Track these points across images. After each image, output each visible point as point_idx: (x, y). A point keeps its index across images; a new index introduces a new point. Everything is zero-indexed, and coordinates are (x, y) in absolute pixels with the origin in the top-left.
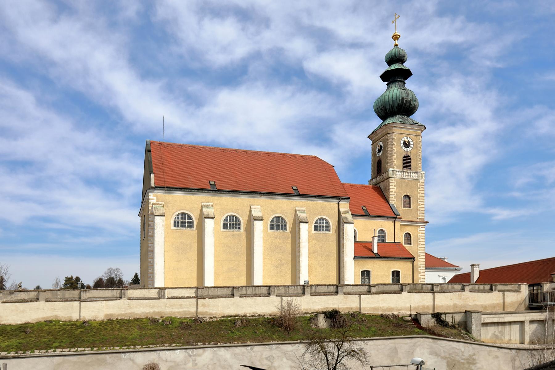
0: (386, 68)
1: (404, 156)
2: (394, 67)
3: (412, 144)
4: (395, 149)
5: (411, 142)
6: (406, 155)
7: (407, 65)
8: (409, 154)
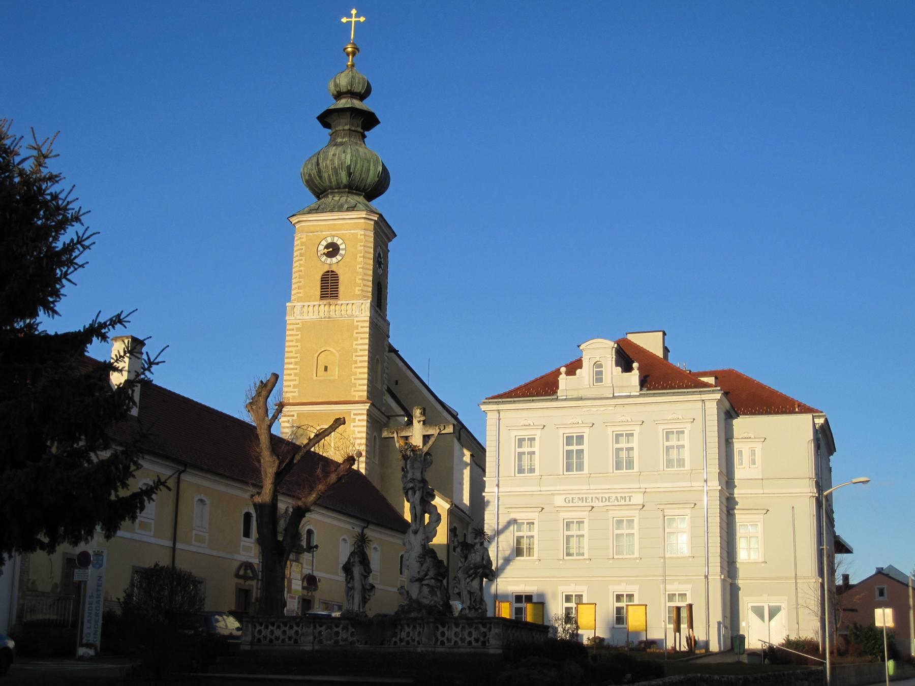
1: (323, 275)
3: (343, 250)
6: (328, 272)
8: (334, 268)
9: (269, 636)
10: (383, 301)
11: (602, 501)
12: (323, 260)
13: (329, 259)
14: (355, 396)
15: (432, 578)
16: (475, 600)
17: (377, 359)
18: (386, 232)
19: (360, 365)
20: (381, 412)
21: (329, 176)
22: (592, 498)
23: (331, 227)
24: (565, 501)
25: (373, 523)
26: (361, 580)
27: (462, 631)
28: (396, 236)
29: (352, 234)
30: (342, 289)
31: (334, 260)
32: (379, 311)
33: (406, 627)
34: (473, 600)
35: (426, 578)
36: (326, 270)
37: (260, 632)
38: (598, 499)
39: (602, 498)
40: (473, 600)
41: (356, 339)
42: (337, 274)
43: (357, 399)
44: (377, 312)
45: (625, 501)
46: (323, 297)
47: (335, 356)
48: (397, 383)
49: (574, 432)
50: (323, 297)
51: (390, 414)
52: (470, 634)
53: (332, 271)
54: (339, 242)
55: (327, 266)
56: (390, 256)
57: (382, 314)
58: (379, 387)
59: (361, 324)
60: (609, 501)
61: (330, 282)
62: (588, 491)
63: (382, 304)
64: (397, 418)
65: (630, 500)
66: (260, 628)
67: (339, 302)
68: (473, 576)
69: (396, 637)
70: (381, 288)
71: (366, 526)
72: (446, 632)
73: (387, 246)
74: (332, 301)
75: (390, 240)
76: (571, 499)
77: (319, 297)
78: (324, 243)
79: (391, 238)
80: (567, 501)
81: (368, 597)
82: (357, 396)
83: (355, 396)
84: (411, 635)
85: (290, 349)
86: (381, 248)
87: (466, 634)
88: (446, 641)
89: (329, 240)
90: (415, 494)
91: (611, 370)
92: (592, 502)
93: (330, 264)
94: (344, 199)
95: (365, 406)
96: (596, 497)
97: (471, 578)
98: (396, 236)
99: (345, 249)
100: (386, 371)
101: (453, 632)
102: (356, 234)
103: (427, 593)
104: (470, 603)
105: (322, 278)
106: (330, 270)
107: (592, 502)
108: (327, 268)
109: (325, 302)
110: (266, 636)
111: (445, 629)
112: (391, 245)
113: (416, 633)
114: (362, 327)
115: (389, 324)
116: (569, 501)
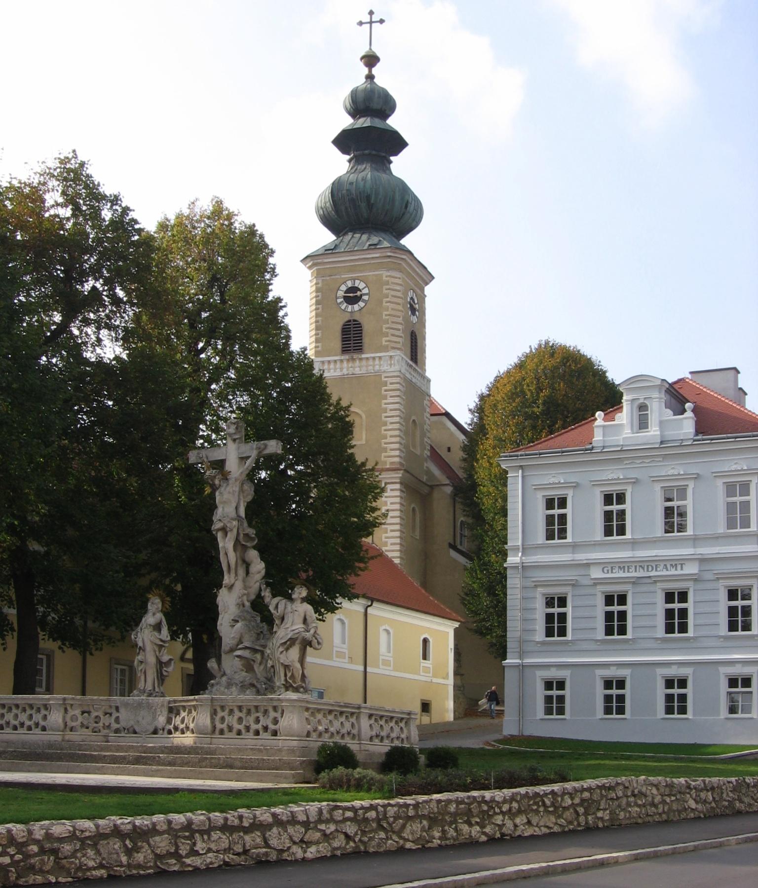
0: (346, 122)
2: (364, 122)
6: (350, 321)
7: (393, 122)
8: (357, 317)
9: (272, 727)
10: (419, 354)
11: (648, 571)
12: (343, 307)
13: (350, 306)
14: (386, 462)
15: (246, 648)
16: (293, 676)
17: (414, 421)
18: (421, 274)
19: (390, 427)
20: (423, 482)
21: (346, 208)
22: (636, 567)
23: (352, 269)
24: (603, 571)
25: (379, 601)
26: (155, 651)
27: (246, 716)
28: (433, 278)
29: (376, 275)
30: (366, 340)
31: (356, 307)
32: (414, 365)
33: (182, 712)
34: (289, 675)
35: (239, 647)
36: (347, 319)
37: (223, 719)
38: (643, 568)
39: (648, 566)
40: (289, 675)
41: (385, 397)
42: (360, 324)
43: (388, 466)
44: (411, 366)
45: (676, 570)
46: (345, 350)
47: (361, 417)
48: (449, 449)
49: (614, 489)
50: (345, 350)
51: (433, 484)
52: (257, 721)
53: (354, 321)
54: (361, 285)
55: (348, 315)
56: (428, 300)
57: (419, 370)
58: (418, 452)
59: (390, 380)
60: (656, 570)
61: (352, 335)
62: (632, 560)
63: (419, 357)
64: (443, 488)
65: (682, 569)
66: (223, 714)
67: (364, 356)
68: (288, 643)
69: (171, 724)
70: (416, 339)
71: (370, 604)
72: (226, 717)
73: (423, 290)
74: (355, 356)
75: (427, 284)
76: (610, 568)
77: (339, 350)
78: (344, 288)
79: (428, 281)
80: (606, 571)
81: (165, 673)
82: (388, 463)
83: (386, 462)
84: (186, 721)
85: (394, 440)
86: (414, 291)
87: (251, 719)
88: (226, 730)
89: (349, 284)
90: (226, 535)
91: (658, 410)
92: (636, 571)
93: (352, 312)
94: (365, 237)
95: (398, 473)
96: (641, 566)
97: (285, 646)
98: (433, 278)
100: (428, 434)
101: (236, 717)
102: (381, 275)
103: (241, 667)
104: (286, 680)
105: (343, 329)
106: (352, 319)
107: (636, 571)
109: (347, 357)
110: (267, 726)
111: (278, 715)
112: (428, 290)
113: (191, 720)
114: (391, 384)
115: (429, 381)
116: (608, 571)
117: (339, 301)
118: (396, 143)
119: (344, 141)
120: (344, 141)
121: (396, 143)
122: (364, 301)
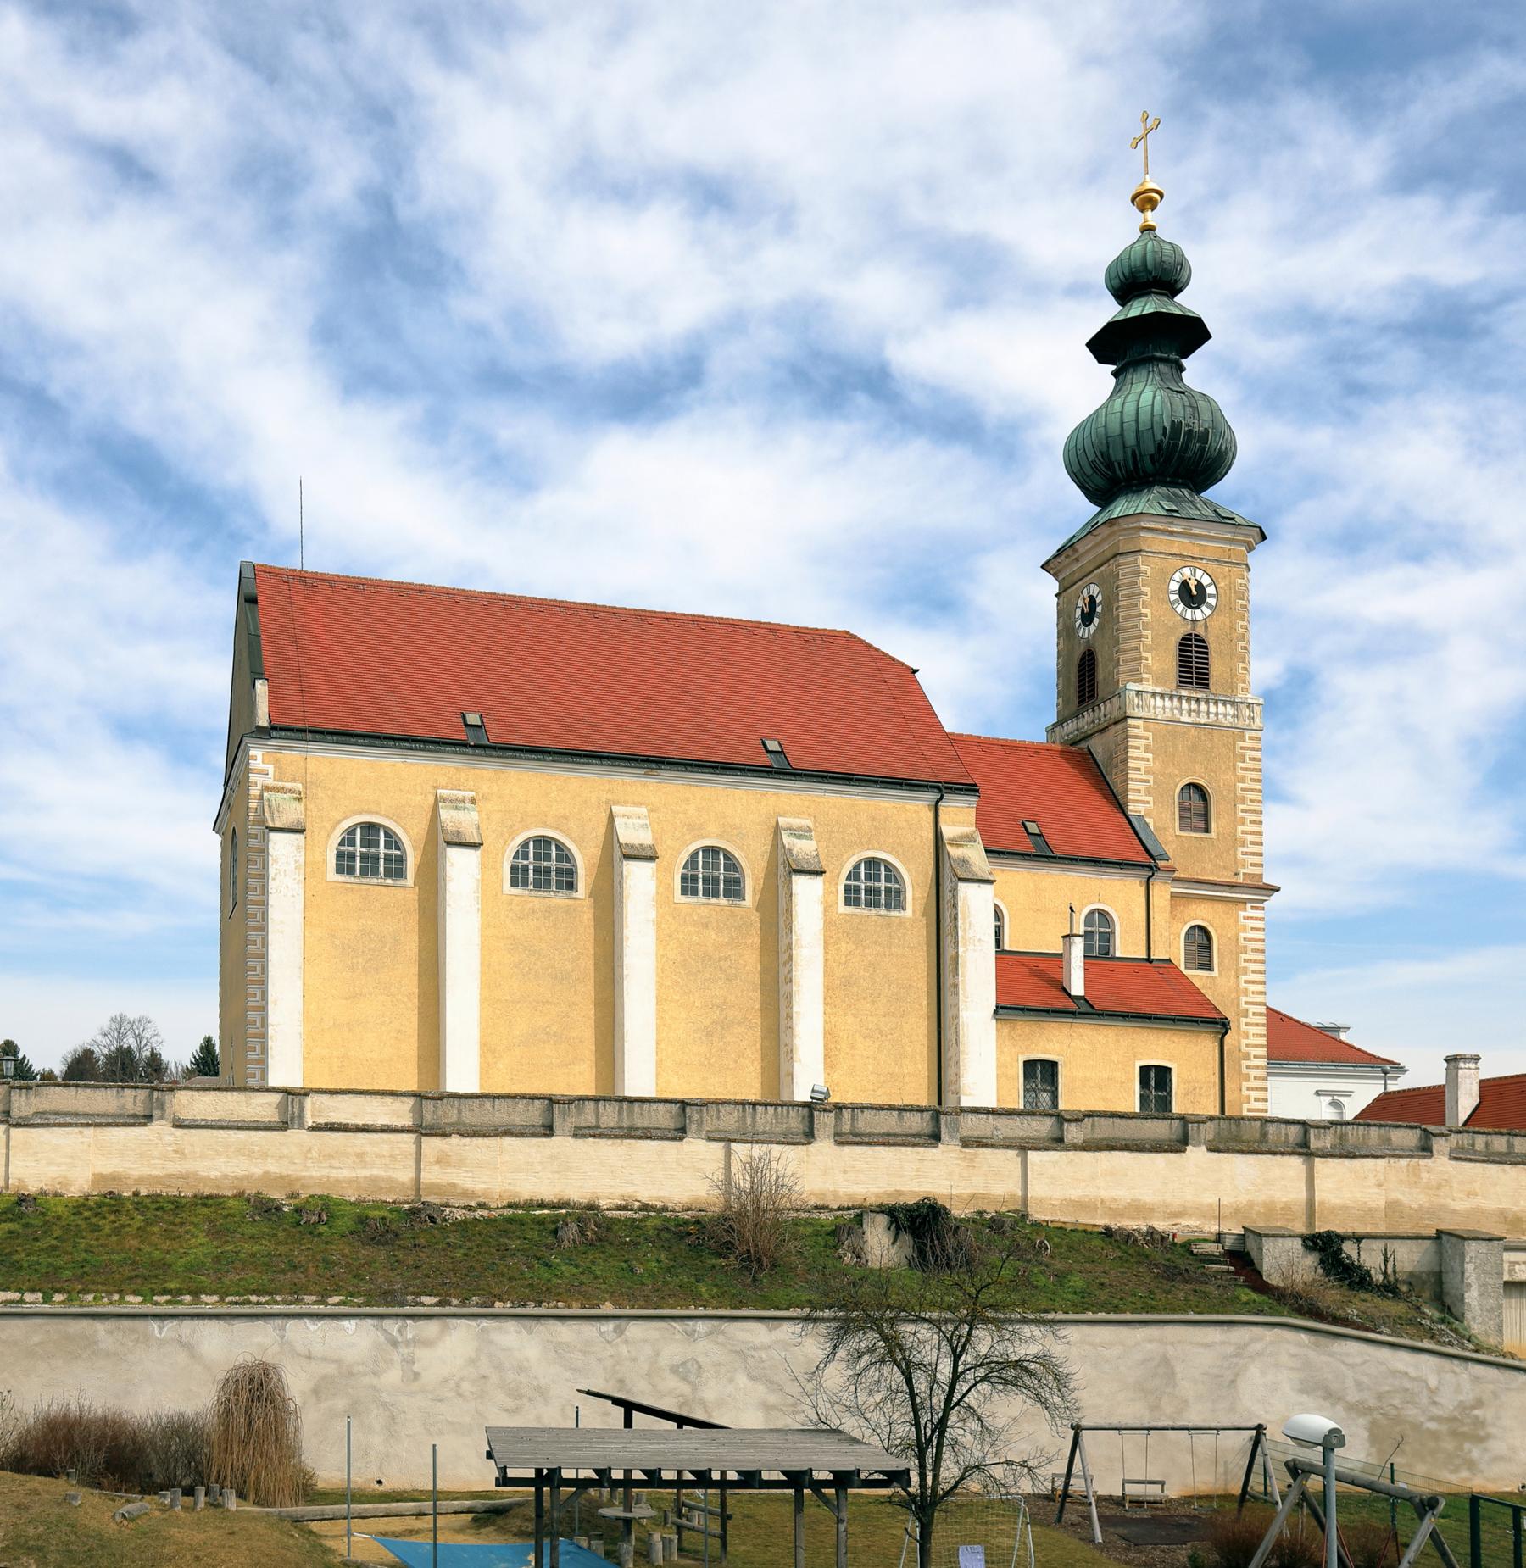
0: (1108, 310)
2: (1137, 309)
4: (1148, 611)
5: (1207, 586)
7: (1189, 301)
8: (1201, 631)
31: (1199, 614)
46: (1185, 680)
50: (1185, 680)
54: (1211, 590)
99: (1172, 603)
108: (1188, 628)
117: (1208, 612)
118: (1192, 333)
119: (1106, 345)
120: (1106, 345)
121: (1192, 333)
122: (1209, 606)
